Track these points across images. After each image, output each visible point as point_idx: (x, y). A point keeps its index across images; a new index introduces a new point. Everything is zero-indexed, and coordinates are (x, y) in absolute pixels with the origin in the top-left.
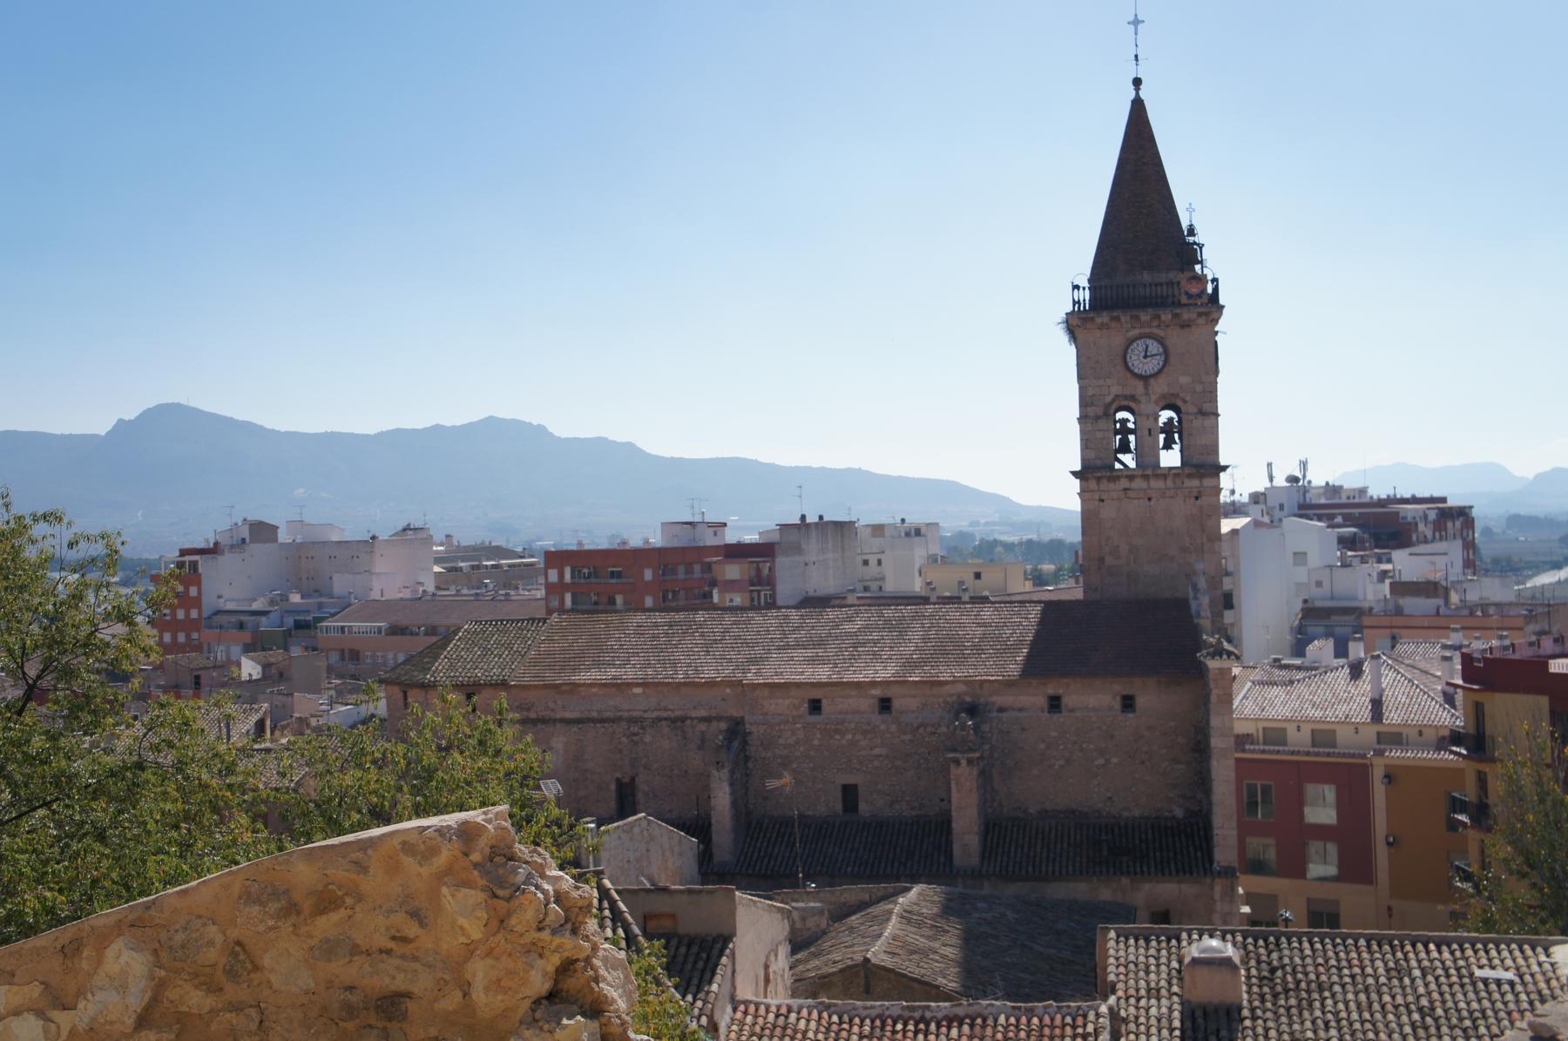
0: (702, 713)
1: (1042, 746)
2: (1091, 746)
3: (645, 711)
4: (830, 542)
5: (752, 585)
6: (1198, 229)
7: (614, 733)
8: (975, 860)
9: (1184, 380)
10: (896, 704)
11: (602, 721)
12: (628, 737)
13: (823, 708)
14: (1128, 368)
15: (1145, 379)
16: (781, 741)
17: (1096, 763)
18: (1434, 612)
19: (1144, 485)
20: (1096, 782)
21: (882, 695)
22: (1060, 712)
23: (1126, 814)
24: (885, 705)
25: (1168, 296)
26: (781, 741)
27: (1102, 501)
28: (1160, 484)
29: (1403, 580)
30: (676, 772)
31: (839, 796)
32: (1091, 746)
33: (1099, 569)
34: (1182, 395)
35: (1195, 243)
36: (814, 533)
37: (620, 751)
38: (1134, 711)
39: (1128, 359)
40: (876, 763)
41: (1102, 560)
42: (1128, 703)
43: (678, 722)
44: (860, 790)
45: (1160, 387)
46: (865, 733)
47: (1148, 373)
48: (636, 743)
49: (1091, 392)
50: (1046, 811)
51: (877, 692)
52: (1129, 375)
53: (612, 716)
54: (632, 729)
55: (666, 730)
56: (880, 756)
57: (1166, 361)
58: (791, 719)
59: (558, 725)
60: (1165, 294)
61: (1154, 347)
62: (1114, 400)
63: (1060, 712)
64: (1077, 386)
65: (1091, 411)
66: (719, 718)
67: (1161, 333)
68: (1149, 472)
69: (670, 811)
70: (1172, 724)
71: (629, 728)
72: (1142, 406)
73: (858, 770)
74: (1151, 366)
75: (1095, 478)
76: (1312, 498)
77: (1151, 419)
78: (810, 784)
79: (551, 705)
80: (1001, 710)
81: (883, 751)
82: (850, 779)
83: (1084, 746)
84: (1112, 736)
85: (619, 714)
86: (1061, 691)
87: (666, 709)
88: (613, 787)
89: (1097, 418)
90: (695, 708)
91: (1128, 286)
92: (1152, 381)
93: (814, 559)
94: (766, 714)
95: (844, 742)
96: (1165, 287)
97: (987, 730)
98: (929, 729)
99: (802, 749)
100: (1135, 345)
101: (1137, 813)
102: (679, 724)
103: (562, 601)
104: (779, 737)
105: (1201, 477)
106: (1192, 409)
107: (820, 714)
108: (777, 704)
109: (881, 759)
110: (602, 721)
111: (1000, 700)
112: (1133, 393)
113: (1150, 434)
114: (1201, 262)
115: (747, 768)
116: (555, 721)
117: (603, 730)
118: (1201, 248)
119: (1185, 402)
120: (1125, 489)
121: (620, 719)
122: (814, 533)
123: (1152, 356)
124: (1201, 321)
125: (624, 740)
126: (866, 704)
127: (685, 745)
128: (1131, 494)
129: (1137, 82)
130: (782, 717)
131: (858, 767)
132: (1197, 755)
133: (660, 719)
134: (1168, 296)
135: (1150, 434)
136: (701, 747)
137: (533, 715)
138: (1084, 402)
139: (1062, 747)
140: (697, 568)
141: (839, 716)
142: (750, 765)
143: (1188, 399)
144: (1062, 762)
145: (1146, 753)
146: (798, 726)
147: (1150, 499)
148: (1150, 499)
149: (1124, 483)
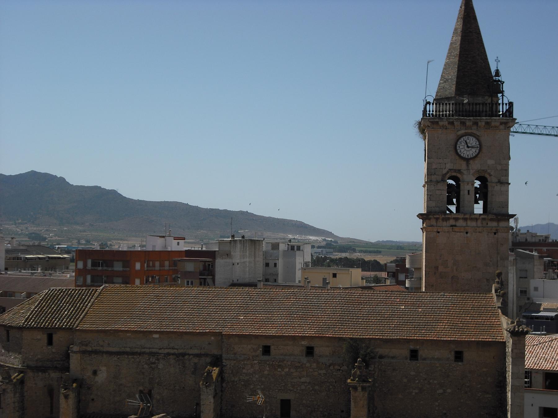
0: (196, 351)
1: (405, 380)
2: (435, 382)
4: (248, 252)
5: (200, 275)
6: (502, 72)
7: (140, 362)
9: (491, 162)
10: (317, 351)
11: (133, 354)
13: (271, 351)
14: (457, 154)
15: (467, 160)
16: (244, 371)
17: (438, 392)
19: (464, 224)
20: (437, 404)
21: (308, 345)
22: (417, 360)
24: (310, 351)
25: (483, 111)
26: (244, 371)
27: (439, 232)
28: (474, 224)
31: (279, 406)
32: (435, 382)
33: (435, 273)
35: (499, 81)
36: (239, 245)
38: (462, 361)
39: (458, 148)
40: (303, 387)
41: (437, 268)
45: (476, 165)
47: (469, 157)
52: (457, 157)
53: (139, 351)
54: (151, 360)
57: (480, 150)
58: (251, 358)
59: (105, 356)
60: (481, 110)
61: (472, 141)
62: (448, 172)
63: (417, 360)
64: (425, 165)
65: (434, 178)
66: (206, 355)
67: (478, 133)
68: (467, 216)
70: (485, 370)
71: (149, 359)
73: (291, 391)
74: (471, 153)
75: (435, 218)
76: (520, 239)
77: (470, 184)
80: (381, 357)
82: (286, 396)
83: (431, 381)
85: (143, 350)
86: (418, 347)
87: (173, 348)
89: (437, 182)
90: (191, 348)
91: (459, 104)
92: (471, 162)
93: (238, 261)
94: (235, 354)
95: (283, 373)
96: (481, 106)
97: (372, 369)
98: (337, 367)
99: (257, 376)
102: (181, 358)
103: (85, 280)
104: (243, 368)
105: (498, 221)
106: (495, 180)
107: (270, 355)
109: (306, 384)
110: (133, 354)
111: (381, 351)
112: (459, 169)
113: (469, 194)
114: (502, 92)
115: (222, 387)
116: (103, 352)
117: (133, 360)
118: (502, 84)
119: (490, 175)
120: (452, 226)
121: (144, 353)
122: (239, 245)
124: (502, 127)
125: (146, 366)
128: (456, 229)
130: (246, 356)
133: (169, 354)
134: (483, 111)
135: (469, 194)
137: (89, 349)
138: (430, 172)
140: (167, 263)
142: (224, 385)
143: (492, 173)
144: (417, 391)
146: (256, 362)
148: (467, 233)
149: (452, 222)
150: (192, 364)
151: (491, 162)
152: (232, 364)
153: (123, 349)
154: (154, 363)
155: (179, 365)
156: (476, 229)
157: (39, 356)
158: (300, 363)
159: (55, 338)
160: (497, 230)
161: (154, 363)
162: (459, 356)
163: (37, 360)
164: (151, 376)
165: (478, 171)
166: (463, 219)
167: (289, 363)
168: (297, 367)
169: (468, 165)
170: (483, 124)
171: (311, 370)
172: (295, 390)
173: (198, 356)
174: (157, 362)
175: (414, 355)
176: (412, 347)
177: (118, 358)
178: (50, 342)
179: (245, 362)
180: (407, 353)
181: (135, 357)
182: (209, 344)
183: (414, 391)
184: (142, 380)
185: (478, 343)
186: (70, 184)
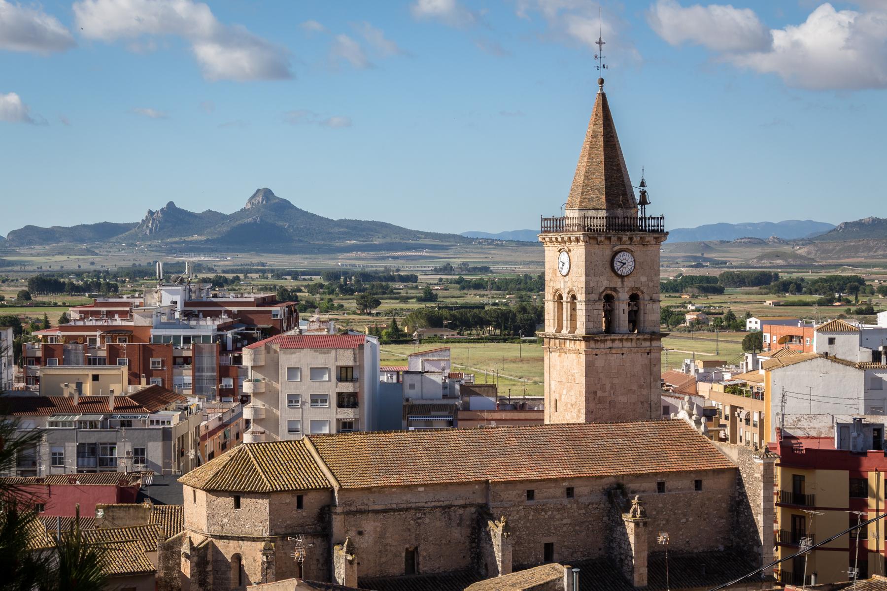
0: (461, 502)
1: (654, 513)
2: (680, 512)
3: (426, 502)
8: (645, 583)
9: (643, 279)
10: (576, 491)
12: (415, 520)
15: (622, 277)
18: (243, 501)
19: (620, 345)
20: (681, 533)
23: (695, 551)
24: (570, 492)
31: (543, 551)
32: (680, 512)
34: (642, 288)
37: (409, 530)
40: (565, 529)
41: (596, 393)
43: (446, 509)
44: (555, 546)
46: (558, 510)
48: (419, 524)
49: (591, 285)
50: (655, 552)
51: (565, 484)
52: (613, 274)
54: (417, 515)
55: (438, 514)
56: (567, 524)
62: (604, 290)
65: (592, 297)
66: (471, 505)
69: (439, 568)
70: (720, 496)
71: (415, 514)
72: (620, 294)
78: (526, 545)
79: (366, 502)
81: (569, 521)
82: (549, 540)
83: (676, 511)
84: (690, 505)
85: (410, 505)
86: (664, 479)
88: (404, 554)
90: (456, 499)
92: (626, 278)
95: (547, 516)
98: (595, 506)
99: (522, 522)
100: (619, 255)
101: (701, 550)
105: (651, 340)
106: (647, 297)
108: (509, 494)
116: (369, 511)
119: (643, 293)
123: (621, 262)
125: (412, 522)
126: (559, 491)
127: (450, 524)
128: (613, 351)
129: (602, 82)
131: (554, 531)
132: (731, 514)
136: (459, 525)
137: (353, 509)
139: (664, 513)
141: (545, 501)
143: (645, 291)
144: (664, 522)
145: (707, 514)
147: (623, 354)
148: (623, 354)
150: (458, 516)
151: (643, 279)
152: (499, 512)
153: (389, 507)
154: (420, 518)
155: (445, 518)
156: (631, 350)
157: (288, 522)
158: (561, 504)
159: (306, 500)
160: (650, 350)
161: (420, 518)
162: (698, 485)
163: (286, 527)
164: (418, 532)
165: (632, 289)
166: (619, 339)
167: (552, 506)
168: (559, 509)
169: (623, 282)
170: (639, 239)
171: (572, 511)
172: (558, 533)
173: (464, 506)
174: (423, 516)
175: (661, 487)
176: (659, 480)
177: (384, 516)
178: (300, 505)
179: (511, 509)
180: (654, 486)
181: (401, 513)
182: (474, 493)
183: (662, 522)
184: (409, 538)
185: (714, 471)
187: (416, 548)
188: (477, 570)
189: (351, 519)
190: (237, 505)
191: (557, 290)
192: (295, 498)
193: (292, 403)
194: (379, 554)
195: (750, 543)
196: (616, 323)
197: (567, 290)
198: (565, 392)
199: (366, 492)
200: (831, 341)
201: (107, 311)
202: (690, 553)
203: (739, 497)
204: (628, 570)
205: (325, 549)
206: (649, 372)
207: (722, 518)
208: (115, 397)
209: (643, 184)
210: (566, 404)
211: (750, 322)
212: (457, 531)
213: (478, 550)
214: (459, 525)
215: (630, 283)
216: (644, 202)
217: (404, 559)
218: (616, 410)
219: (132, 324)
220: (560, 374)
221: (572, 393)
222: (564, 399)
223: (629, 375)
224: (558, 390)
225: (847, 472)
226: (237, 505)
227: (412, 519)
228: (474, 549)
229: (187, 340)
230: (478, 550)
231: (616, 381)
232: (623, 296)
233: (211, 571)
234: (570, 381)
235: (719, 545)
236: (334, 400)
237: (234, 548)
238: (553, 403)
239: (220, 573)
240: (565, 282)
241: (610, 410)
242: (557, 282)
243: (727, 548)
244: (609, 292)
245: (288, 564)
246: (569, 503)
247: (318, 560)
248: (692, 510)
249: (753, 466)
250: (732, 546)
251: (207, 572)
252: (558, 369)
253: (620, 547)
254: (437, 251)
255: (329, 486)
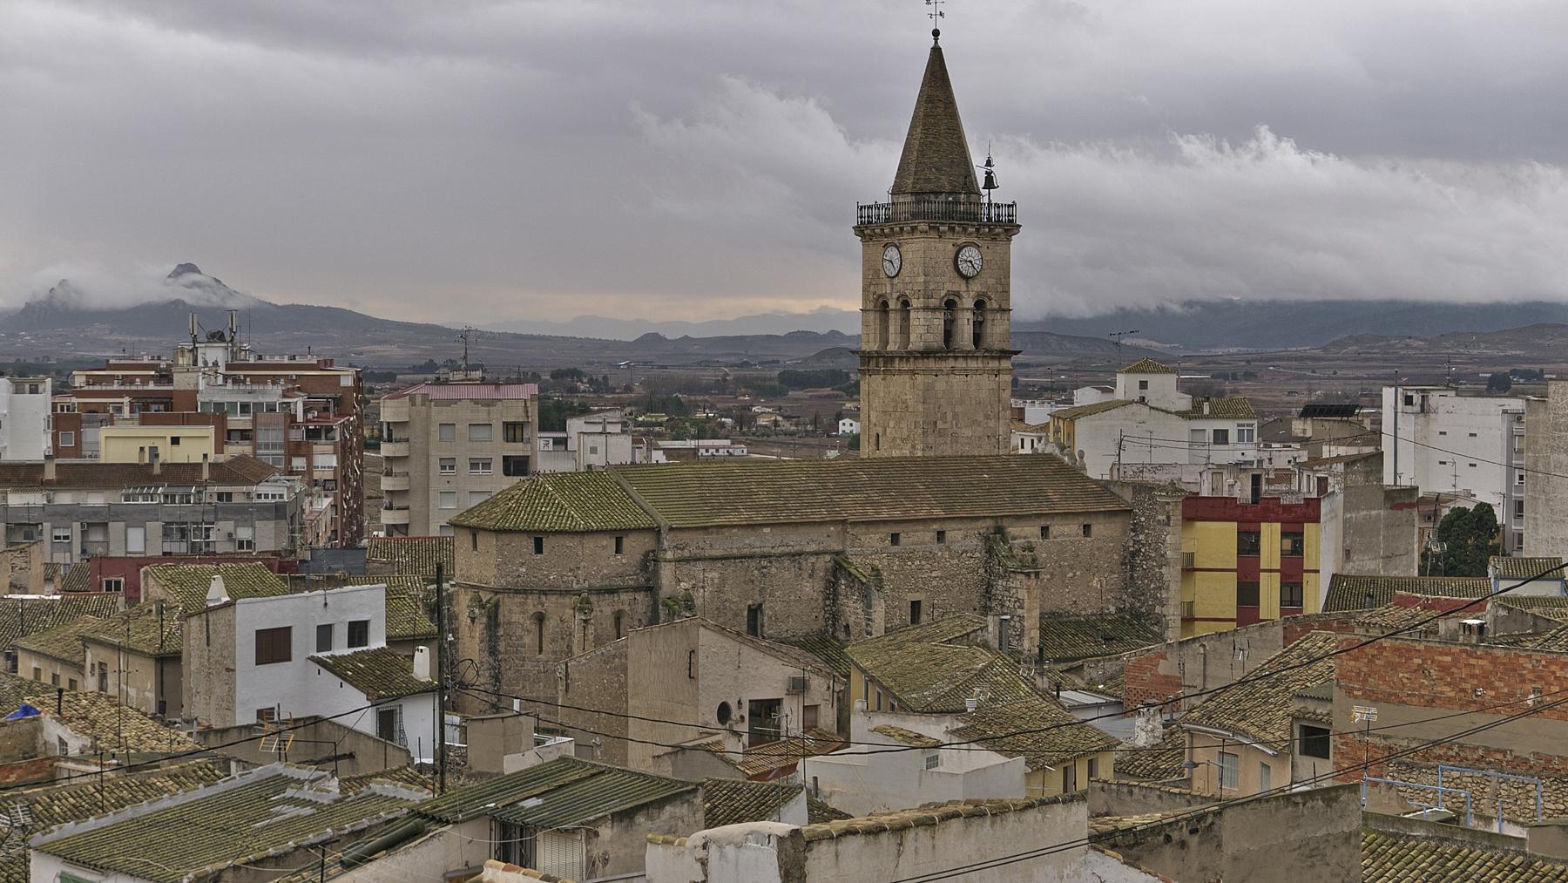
3: (773, 547)
10: (949, 535)
15: (966, 278)
18: (547, 543)
29: (190, 462)
30: (792, 598)
40: (934, 583)
42: (1087, 529)
46: (926, 558)
62: (946, 295)
69: (787, 631)
84: (1078, 556)
86: (1049, 523)
88: (746, 613)
119: (990, 299)
125: (756, 572)
127: (800, 575)
129: (936, 33)
136: (811, 576)
137: (686, 554)
144: (1048, 576)
147: (967, 376)
148: (967, 376)
155: (794, 567)
186: (824, 335)
187: (761, 605)
188: (832, 634)
189: (685, 567)
190: (539, 550)
191: (880, 296)
192: (614, 540)
193: (446, 469)
194: (717, 612)
195: (1150, 603)
196: (959, 337)
197: (895, 295)
198: (892, 424)
199: (701, 532)
200: (1143, 385)
201: (123, 376)
202: (1077, 616)
203: (1133, 547)
204: (1014, 633)
205: (648, 606)
206: (997, 399)
207: (1114, 573)
208: (209, 464)
209: (989, 163)
210: (894, 439)
211: (844, 424)
212: (808, 584)
213: (834, 609)
214: (811, 576)
215: (976, 287)
216: (990, 183)
217: (746, 619)
218: (958, 446)
219: (171, 388)
220: (884, 402)
221: (903, 425)
222: (891, 433)
223: (974, 402)
224: (881, 422)
225: (1235, 525)
226: (539, 550)
227: (756, 569)
228: (829, 608)
229: (245, 408)
230: (834, 609)
231: (958, 409)
232: (968, 302)
233: (502, 636)
234: (899, 410)
235: (1110, 606)
236: (498, 466)
237: (534, 606)
238: (873, 440)
239: (514, 638)
240: (892, 284)
241: (952, 447)
242: (880, 286)
243: (1119, 610)
244: (951, 297)
245: (604, 625)
246: (940, 550)
247: (640, 620)
248: (1080, 562)
249: (1156, 507)
250: (1124, 607)
251: (498, 637)
252: (882, 394)
253: (1003, 606)
254: (28, 462)
255: (656, 525)
